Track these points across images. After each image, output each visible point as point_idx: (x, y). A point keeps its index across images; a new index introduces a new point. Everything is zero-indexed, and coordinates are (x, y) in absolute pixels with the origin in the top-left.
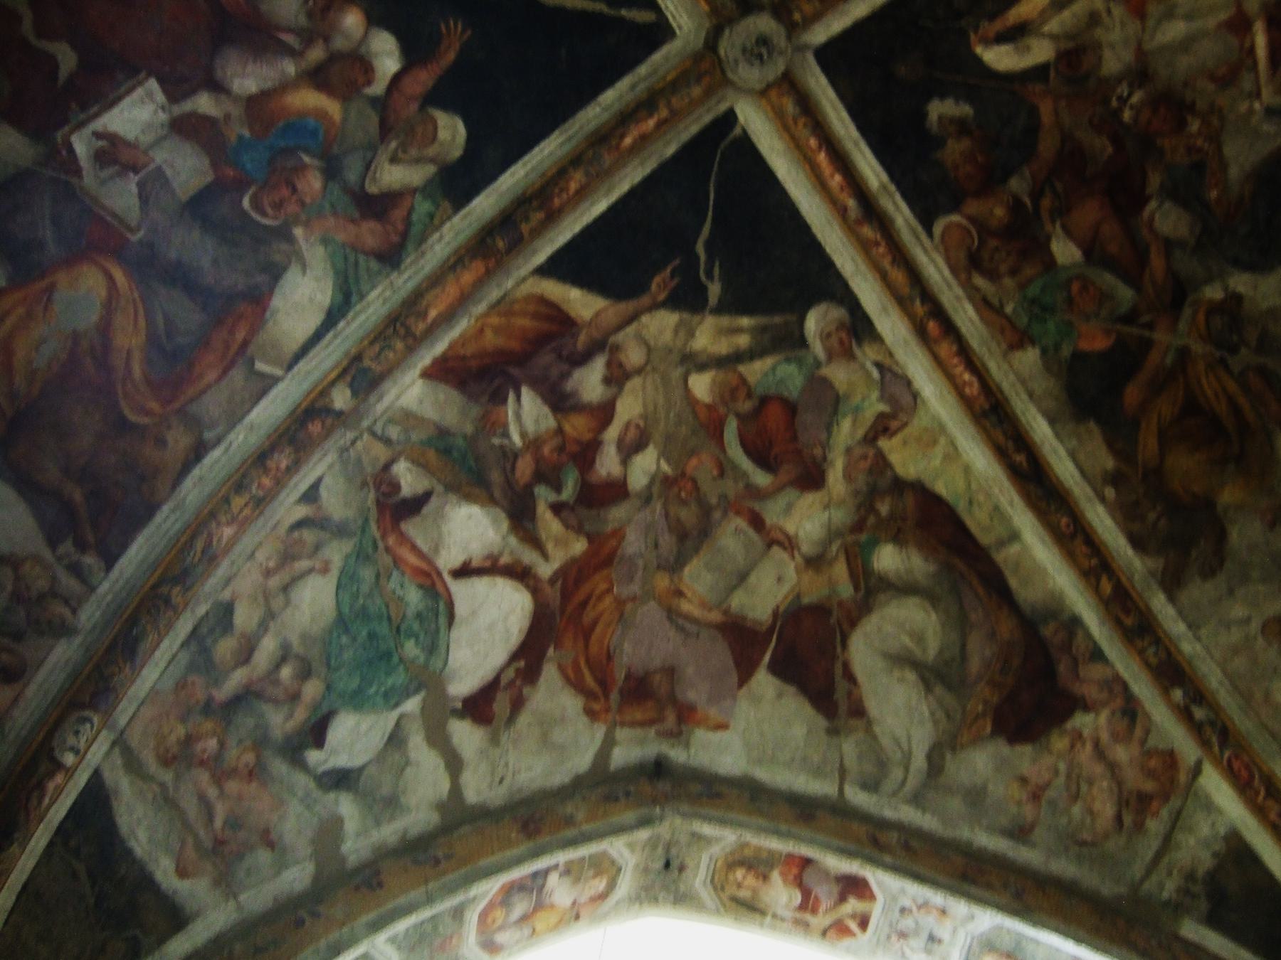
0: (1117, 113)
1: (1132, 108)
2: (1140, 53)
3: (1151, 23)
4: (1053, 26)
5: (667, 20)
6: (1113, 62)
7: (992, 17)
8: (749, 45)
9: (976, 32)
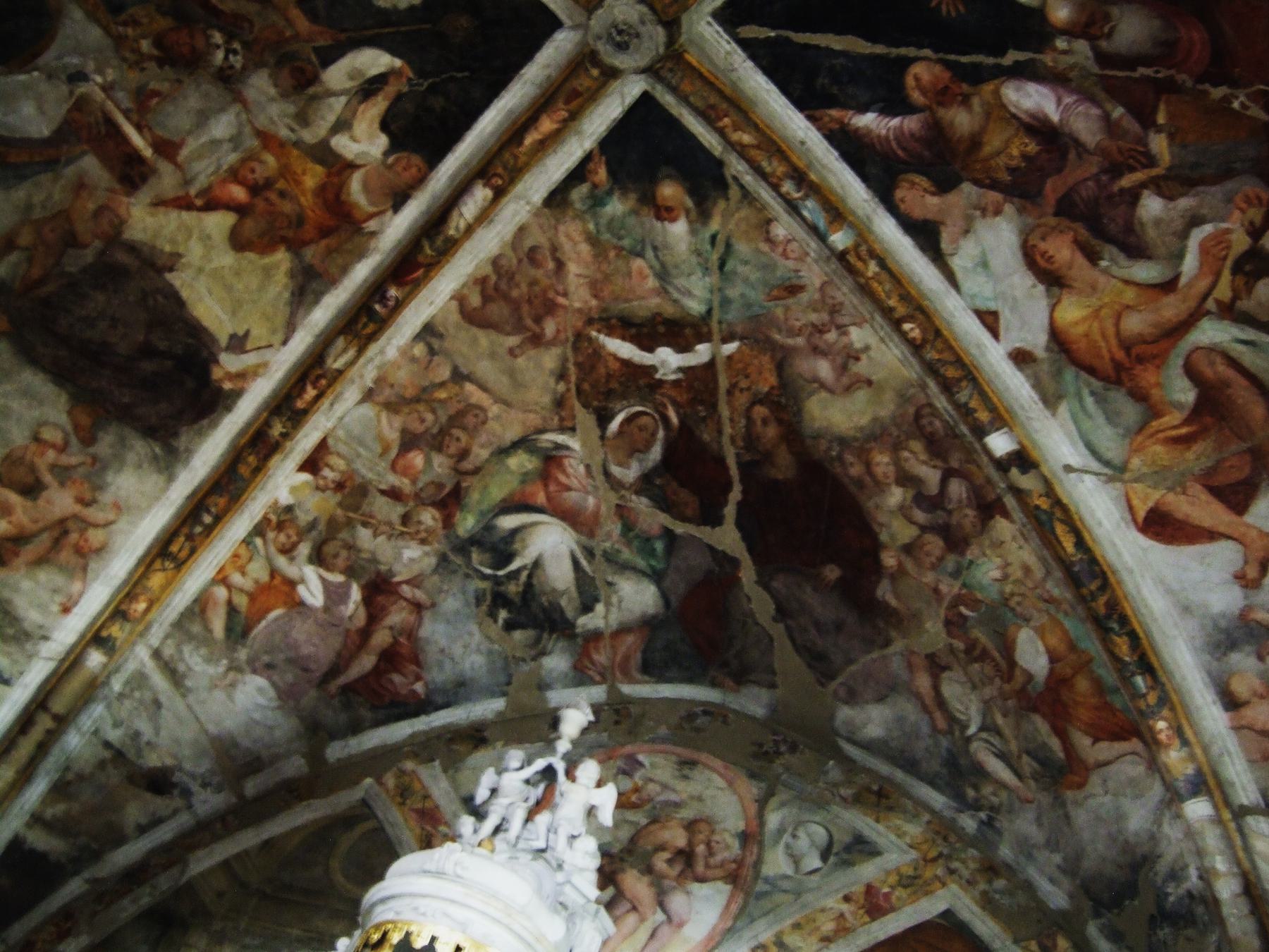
0: (230, 38)
1: (218, 47)
2: (239, 98)
3: (247, 130)
4: (338, 104)
5: (725, 30)
6: (260, 85)
7: (399, 97)
8: (635, 41)
9: (410, 80)
